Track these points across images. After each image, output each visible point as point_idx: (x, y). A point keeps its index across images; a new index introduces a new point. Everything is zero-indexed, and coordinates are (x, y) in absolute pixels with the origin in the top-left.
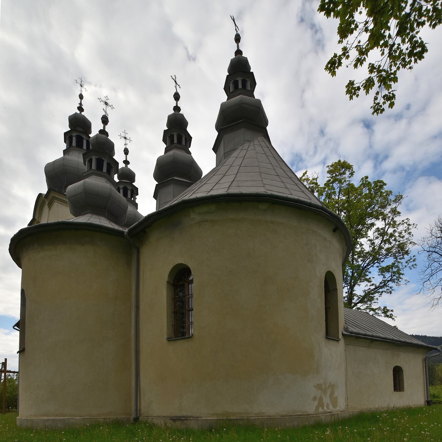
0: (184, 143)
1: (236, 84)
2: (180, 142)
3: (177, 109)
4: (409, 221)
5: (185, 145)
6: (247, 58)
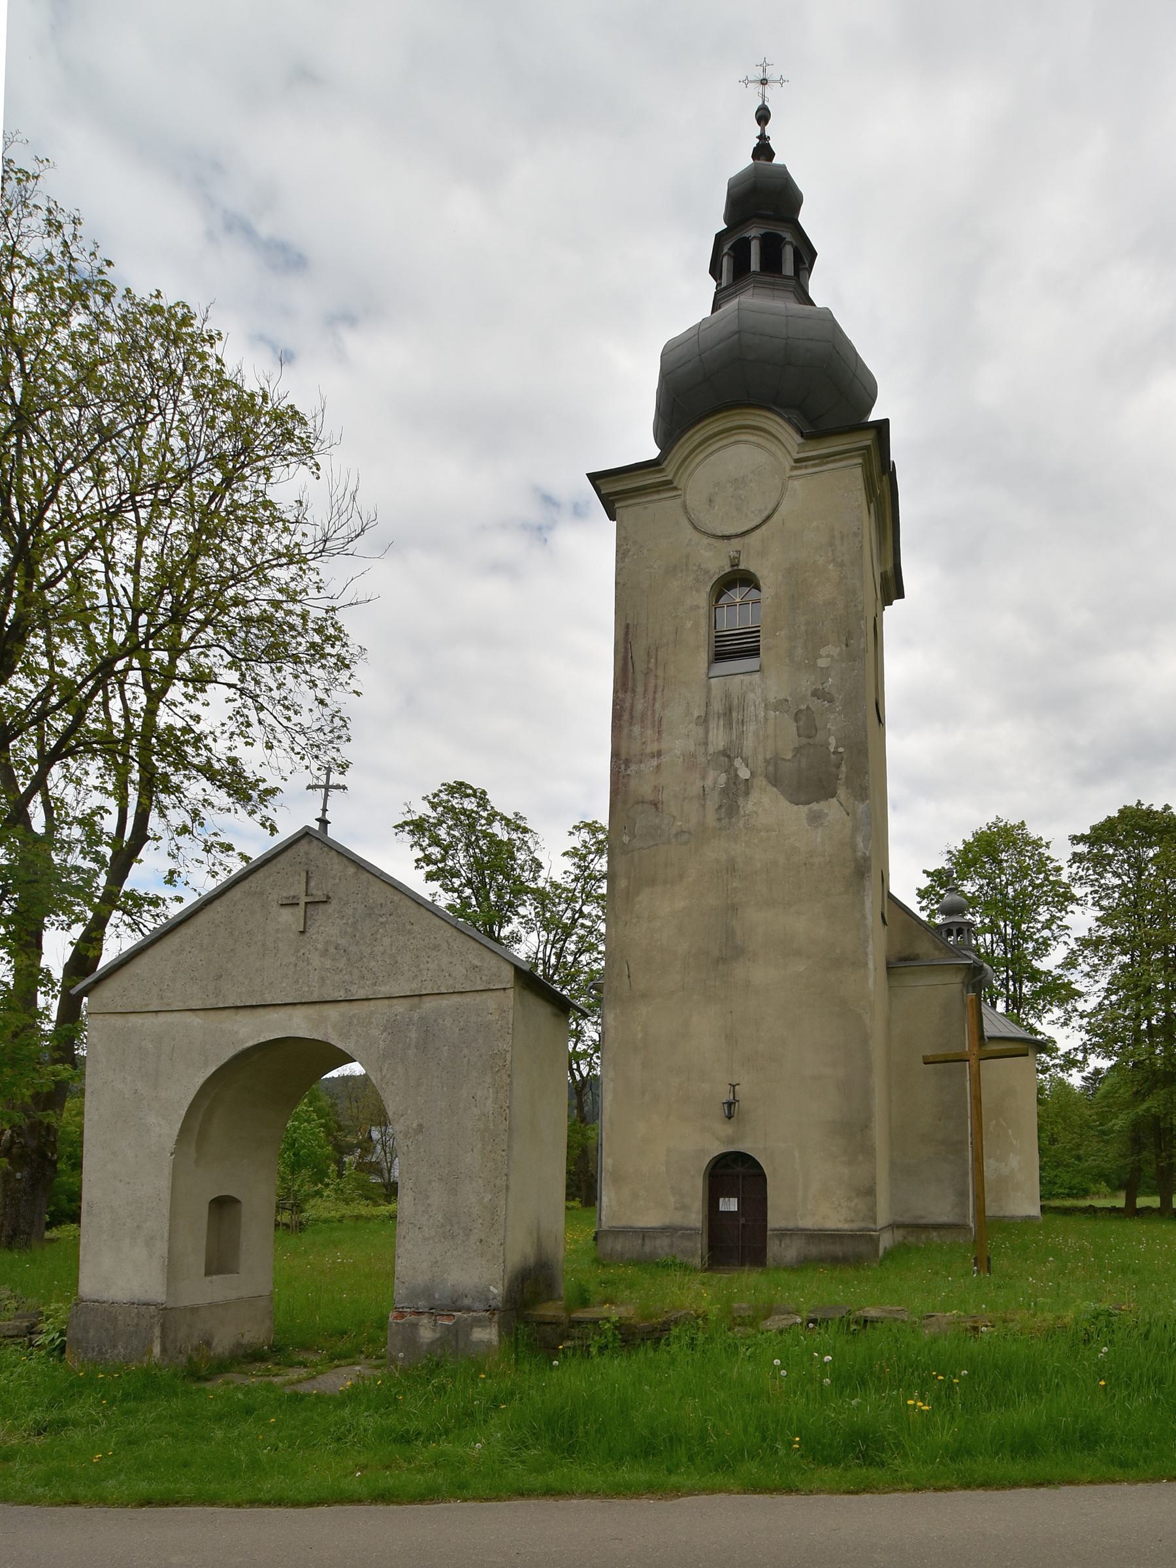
0: (788, 268)
1: (740, 253)
2: (771, 263)
3: (763, 150)
4: (80, 231)
5: (792, 274)
6: (784, 167)
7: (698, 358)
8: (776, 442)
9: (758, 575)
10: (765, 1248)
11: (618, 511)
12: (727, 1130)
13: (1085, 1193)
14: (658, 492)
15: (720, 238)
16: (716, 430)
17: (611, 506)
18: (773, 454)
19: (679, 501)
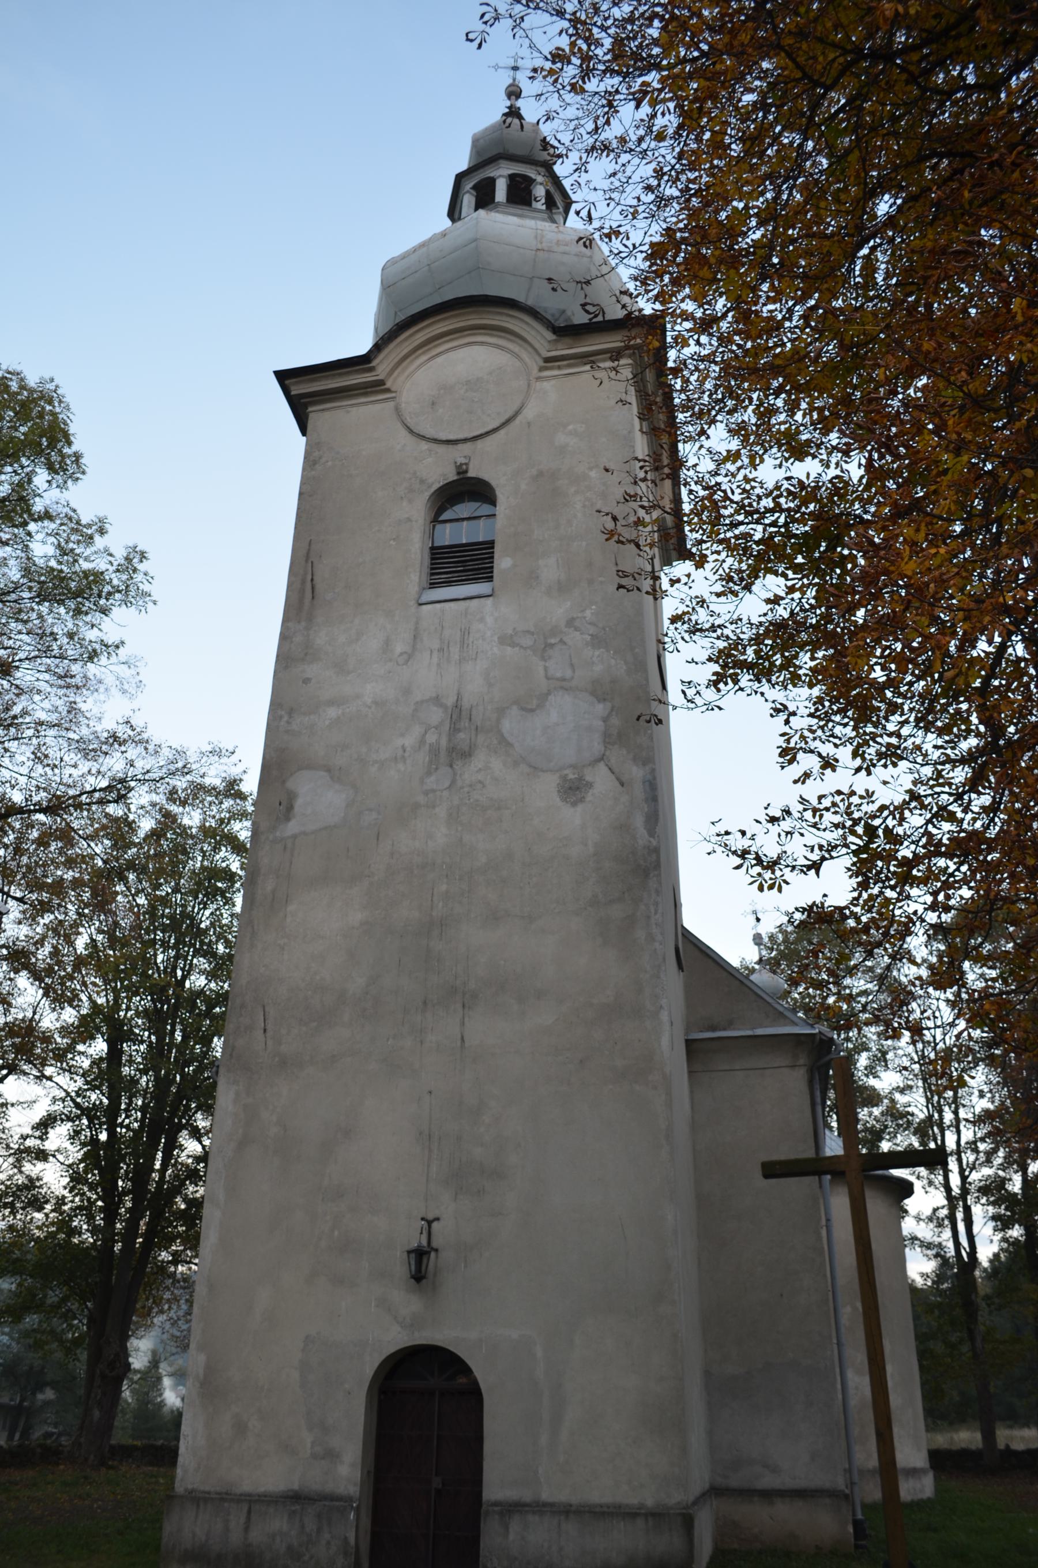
8: (520, 342)
9: (493, 483)
11: (311, 415)
13: (729, 1025)
14: (366, 394)
15: (460, 178)
16: (445, 329)
18: (517, 356)
19: (392, 404)
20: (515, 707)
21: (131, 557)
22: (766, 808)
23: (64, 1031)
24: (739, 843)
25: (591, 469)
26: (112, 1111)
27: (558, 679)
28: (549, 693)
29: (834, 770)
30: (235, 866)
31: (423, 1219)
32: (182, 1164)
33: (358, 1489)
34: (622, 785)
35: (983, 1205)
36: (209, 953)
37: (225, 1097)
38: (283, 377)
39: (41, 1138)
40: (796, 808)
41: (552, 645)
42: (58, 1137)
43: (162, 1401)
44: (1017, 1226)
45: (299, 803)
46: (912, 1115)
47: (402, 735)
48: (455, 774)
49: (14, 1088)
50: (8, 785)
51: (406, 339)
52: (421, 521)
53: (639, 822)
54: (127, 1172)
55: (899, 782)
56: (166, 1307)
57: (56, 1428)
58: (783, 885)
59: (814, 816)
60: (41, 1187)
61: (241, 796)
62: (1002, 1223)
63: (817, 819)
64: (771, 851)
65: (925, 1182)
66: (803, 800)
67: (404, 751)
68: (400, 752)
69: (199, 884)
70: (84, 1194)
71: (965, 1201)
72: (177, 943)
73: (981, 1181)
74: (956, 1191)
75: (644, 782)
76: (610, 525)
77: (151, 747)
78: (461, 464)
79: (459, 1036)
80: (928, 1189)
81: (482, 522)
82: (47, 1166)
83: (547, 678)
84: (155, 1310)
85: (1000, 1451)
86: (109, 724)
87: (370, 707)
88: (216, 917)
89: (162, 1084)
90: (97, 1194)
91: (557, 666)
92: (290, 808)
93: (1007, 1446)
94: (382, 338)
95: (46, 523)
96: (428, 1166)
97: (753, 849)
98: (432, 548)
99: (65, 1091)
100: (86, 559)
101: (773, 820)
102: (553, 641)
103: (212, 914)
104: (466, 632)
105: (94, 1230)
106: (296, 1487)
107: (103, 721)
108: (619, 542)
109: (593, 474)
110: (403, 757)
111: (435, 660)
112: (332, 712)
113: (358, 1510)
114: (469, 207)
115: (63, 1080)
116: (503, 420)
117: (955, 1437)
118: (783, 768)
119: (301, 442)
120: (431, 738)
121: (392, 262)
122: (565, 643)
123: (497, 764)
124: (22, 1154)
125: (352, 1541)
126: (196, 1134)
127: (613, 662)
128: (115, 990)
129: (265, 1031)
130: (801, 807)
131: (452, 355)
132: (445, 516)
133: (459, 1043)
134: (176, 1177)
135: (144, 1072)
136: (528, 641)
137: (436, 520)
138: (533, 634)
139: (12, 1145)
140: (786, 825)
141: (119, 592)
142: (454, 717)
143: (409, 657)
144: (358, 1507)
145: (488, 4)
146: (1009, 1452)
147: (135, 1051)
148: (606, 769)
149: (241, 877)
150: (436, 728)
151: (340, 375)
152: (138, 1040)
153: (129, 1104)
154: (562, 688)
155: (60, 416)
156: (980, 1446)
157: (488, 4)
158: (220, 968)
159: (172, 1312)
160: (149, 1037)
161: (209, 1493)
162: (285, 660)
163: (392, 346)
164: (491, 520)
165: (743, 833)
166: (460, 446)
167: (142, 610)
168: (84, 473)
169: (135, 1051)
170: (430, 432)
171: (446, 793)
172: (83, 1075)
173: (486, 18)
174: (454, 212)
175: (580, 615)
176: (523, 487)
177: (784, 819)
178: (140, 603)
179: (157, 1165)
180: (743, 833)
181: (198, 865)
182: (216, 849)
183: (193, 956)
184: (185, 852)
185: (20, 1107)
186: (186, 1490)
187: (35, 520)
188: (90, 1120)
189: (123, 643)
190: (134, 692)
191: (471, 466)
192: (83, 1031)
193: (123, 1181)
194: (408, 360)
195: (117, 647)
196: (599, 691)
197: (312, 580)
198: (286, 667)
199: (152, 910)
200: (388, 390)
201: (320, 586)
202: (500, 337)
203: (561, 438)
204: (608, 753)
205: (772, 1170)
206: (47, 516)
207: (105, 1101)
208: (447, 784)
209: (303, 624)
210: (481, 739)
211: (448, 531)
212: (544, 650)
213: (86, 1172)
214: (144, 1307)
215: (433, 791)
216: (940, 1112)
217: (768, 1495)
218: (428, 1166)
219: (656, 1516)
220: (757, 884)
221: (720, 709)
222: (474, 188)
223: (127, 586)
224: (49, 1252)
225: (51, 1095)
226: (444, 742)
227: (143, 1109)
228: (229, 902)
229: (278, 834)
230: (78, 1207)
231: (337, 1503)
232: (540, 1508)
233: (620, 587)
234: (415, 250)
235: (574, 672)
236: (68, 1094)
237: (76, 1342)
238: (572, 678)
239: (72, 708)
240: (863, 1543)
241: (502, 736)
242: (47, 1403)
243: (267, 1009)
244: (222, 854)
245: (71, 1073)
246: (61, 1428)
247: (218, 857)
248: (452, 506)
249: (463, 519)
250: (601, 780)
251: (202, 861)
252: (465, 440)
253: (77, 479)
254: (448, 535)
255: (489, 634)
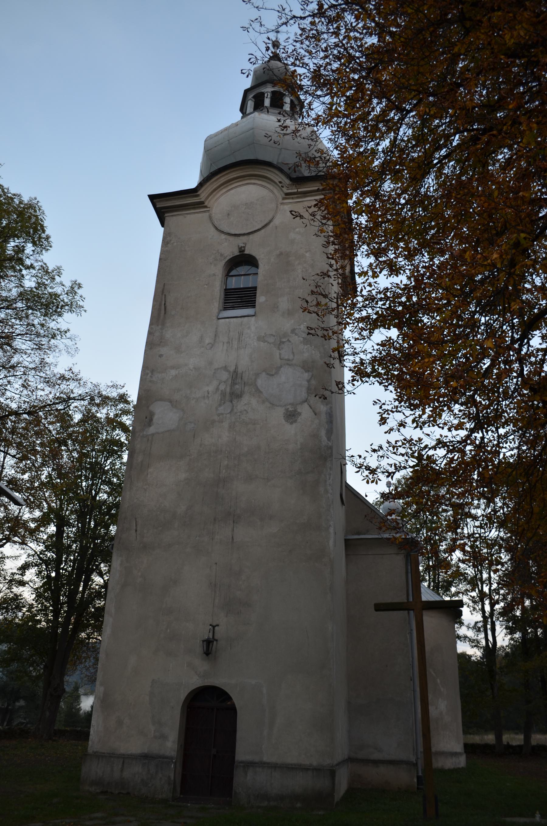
7: (227, 142)
8: (273, 184)
9: (257, 257)
10: (232, 779)
11: (166, 218)
12: (202, 665)
13: (367, 532)
14: (194, 208)
15: (246, 92)
16: (235, 176)
17: (161, 215)
18: (272, 191)
19: (207, 214)
20: (264, 373)
21: (74, 286)
22: (371, 445)
23: (34, 520)
24: (358, 461)
25: (306, 252)
26: (58, 561)
27: (286, 360)
28: (281, 367)
29: (404, 427)
30: (123, 439)
31: (211, 625)
32: (93, 589)
33: (176, 753)
34: (316, 414)
35: (500, 621)
36: (109, 483)
37: (116, 561)
38: (153, 198)
39: (22, 575)
40: (385, 445)
41: (284, 342)
42: (30, 574)
43: (80, 708)
44: (518, 633)
45: (155, 418)
46: (467, 574)
47: (208, 385)
48: (233, 406)
49: (9, 549)
50: (9, 400)
51: (215, 181)
52: (220, 276)
53: (323, 433)
54: (65, 593)
55: (434, 434)
56: (84, 660)
57: (25, 720)
58: (378, 481)
59: (394, 450)
60: (22, 599)
61: (127, 402)
62: (511, 631)
63: (395, 450)
64: (373, 466)
65: (472, 609)
66: (388, 442)
67: (208, 393)
68: (206, 394)
69: (105, 447)
70: (43, 603)
71: (492, 619)
72: (93, 477)
73: (500, 609)
74: (487, 614)
75: (326, 414)
76: (305, 305)
77: (82, 382)
78: (242, 247)
79: (231, 537)
80: (473, 612)
81: (251, 277)
82: (24, 589)
83: (281, 359)
84: (78, 662)
85: (505, 745)
86: (60, 370)
87: (192, 371)
88: (113, 464)
89: (83, 550)
90: (50, 603)
91: (286, 353)
92: (151, 420)
93: (508, 743)
94: (203, 180)
95: (31, 270)
96: (214, 600)
97: (365, 464)
98: (226, 290)
99: (34, 551)
100: (51, 288)
101: (374, 451)
102: (284, 340)
103: (111, 462)
104: (241, 334)
105: (48, 621)
106: (146, 751)
107: (57, 366)
108: (309, 312)
109: (307, 255)
110: (208, 397)
111: (225, 347)
112: (173, 372)
113: (175, 764)
114: (251, 107)
115: (33, 545)
116: (263, 224)
117: (486, 737)
118: (380, 425)
119: (161, 230)
120: (222, 387)
121: (210, 138)
122: (290, 341)
123: (254, 402)
124: (11, 582)
125: (172, 778)
126: (101, 575)
127: (314, 352)
128: (61, 500)
129: (136, 531)
130: (387, 445)
131: (239, 189)
132: (232, 273)
133: (231, 540)
134: (90, 595)
135: (74, 542)
136: (271, 340)
137: (228, 275)
138: (274, 336)
139: (7, 578)
140: (381, 453)
141: (67, 305)
142: (234, 377)
143: (212, 346)
144: (176, 761)
145: (252, 54)
146: (509, 746)
147: (71, 531)
148: (308, 406)
149: (126, 444)
150: (225, 382)
151: (182, 198)
152: (70, 525)
153: (66, 558)
154: (288, 364)
155: (39, 217)
156: (522, 743)
157: (252, 54)
158: (115, 490)
159: (87, 663)
160: (78, 524)
161: (104, 753)
162: (150, 345)
163: (208, 184)
164: (255, 276)
165: (360, 456)
166: (241, 238)
167: (79, 314)
168: (51, 247)
169: (71, 531)
170: (226, 230)
171: (228, 416)
172: (44, 543)
173: (251, 61)
174: (243, 109)
175: (298, 327)
176: (272, 260)
177: (379, 451)
178: (78, 311)
179: (81, 589)
180: (360, 456)
181: (104, 438)
182: (114, 429)
183: (101, 484)
184: (98, 432)
185: (11, 559)
186: (93, 752)
187: (26, 269)
188: (47, 567)
189: (69, 330)
190: (73, 353)
191: (246, 248)
192: (44, 521)
193: (63, 597)
194: (216, 191)
195: (66, 332)
196: (307, 366)
197: (165, 304)
198: (151, 348)
199: (79, 460)
200: (206, 207)
201: (168, 308)
202: (264, 181)
203: (292, 235)
204: (309, 398)
205: (379, 607)
206: (32, 267)
207: (55, 556)
208: (229, 411)
209: (160, 327)
210: (246, 388)
211: (234, 281)
212: (280, 345)
213: (44, 592)
214: (72, 660)
215: (222, 414)
216: (481, 573)
217: (376, 763)
218: (214, 600)
219: (317, 770)
220: (366, 480)
221: (354, 394)
222: (254, 97)
223: (71, 303)
224: (25, 632)
225: (27, 553)
226: (228, 390)
227: (74, 561)
228: (120, 457)
229: (145, 433)
230: (40, 610)
231: (166, 760)
232: (263, 765)
233: (309, 334)
234: (222, 132)
235: (294, 356)
236: (36, 553)
237: (38, 677)
238: (293, 359)
239: (42, 361)
240: (421, 787)
241: (257, 388)
242: (21, 707)
243: (137, 520)
244: (117, 432)
245: (37, 542)
246: (28, 720)
247: (114, 433)
248: (236, 268)
249: (242, 275)
250: (305, 411)
251: (106, 436)
252: (244, 235)
253: (48, 249)
254: (233, 283)
255: (252, 335)
